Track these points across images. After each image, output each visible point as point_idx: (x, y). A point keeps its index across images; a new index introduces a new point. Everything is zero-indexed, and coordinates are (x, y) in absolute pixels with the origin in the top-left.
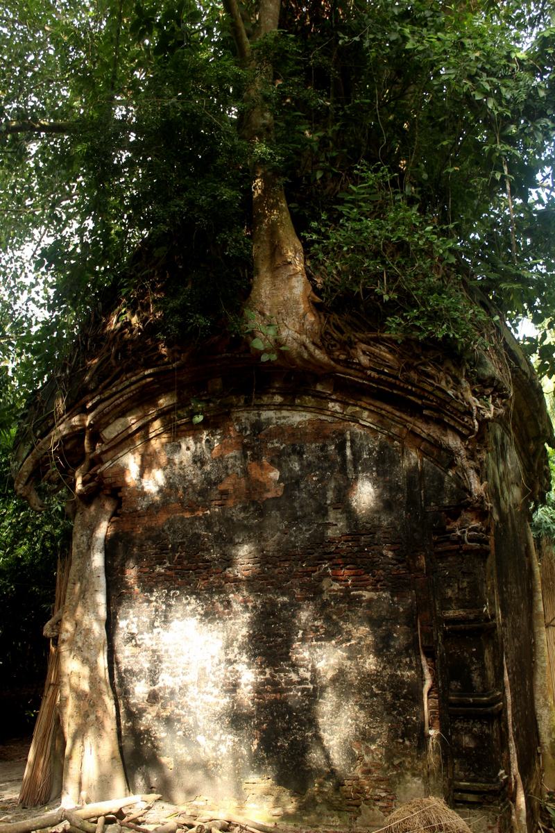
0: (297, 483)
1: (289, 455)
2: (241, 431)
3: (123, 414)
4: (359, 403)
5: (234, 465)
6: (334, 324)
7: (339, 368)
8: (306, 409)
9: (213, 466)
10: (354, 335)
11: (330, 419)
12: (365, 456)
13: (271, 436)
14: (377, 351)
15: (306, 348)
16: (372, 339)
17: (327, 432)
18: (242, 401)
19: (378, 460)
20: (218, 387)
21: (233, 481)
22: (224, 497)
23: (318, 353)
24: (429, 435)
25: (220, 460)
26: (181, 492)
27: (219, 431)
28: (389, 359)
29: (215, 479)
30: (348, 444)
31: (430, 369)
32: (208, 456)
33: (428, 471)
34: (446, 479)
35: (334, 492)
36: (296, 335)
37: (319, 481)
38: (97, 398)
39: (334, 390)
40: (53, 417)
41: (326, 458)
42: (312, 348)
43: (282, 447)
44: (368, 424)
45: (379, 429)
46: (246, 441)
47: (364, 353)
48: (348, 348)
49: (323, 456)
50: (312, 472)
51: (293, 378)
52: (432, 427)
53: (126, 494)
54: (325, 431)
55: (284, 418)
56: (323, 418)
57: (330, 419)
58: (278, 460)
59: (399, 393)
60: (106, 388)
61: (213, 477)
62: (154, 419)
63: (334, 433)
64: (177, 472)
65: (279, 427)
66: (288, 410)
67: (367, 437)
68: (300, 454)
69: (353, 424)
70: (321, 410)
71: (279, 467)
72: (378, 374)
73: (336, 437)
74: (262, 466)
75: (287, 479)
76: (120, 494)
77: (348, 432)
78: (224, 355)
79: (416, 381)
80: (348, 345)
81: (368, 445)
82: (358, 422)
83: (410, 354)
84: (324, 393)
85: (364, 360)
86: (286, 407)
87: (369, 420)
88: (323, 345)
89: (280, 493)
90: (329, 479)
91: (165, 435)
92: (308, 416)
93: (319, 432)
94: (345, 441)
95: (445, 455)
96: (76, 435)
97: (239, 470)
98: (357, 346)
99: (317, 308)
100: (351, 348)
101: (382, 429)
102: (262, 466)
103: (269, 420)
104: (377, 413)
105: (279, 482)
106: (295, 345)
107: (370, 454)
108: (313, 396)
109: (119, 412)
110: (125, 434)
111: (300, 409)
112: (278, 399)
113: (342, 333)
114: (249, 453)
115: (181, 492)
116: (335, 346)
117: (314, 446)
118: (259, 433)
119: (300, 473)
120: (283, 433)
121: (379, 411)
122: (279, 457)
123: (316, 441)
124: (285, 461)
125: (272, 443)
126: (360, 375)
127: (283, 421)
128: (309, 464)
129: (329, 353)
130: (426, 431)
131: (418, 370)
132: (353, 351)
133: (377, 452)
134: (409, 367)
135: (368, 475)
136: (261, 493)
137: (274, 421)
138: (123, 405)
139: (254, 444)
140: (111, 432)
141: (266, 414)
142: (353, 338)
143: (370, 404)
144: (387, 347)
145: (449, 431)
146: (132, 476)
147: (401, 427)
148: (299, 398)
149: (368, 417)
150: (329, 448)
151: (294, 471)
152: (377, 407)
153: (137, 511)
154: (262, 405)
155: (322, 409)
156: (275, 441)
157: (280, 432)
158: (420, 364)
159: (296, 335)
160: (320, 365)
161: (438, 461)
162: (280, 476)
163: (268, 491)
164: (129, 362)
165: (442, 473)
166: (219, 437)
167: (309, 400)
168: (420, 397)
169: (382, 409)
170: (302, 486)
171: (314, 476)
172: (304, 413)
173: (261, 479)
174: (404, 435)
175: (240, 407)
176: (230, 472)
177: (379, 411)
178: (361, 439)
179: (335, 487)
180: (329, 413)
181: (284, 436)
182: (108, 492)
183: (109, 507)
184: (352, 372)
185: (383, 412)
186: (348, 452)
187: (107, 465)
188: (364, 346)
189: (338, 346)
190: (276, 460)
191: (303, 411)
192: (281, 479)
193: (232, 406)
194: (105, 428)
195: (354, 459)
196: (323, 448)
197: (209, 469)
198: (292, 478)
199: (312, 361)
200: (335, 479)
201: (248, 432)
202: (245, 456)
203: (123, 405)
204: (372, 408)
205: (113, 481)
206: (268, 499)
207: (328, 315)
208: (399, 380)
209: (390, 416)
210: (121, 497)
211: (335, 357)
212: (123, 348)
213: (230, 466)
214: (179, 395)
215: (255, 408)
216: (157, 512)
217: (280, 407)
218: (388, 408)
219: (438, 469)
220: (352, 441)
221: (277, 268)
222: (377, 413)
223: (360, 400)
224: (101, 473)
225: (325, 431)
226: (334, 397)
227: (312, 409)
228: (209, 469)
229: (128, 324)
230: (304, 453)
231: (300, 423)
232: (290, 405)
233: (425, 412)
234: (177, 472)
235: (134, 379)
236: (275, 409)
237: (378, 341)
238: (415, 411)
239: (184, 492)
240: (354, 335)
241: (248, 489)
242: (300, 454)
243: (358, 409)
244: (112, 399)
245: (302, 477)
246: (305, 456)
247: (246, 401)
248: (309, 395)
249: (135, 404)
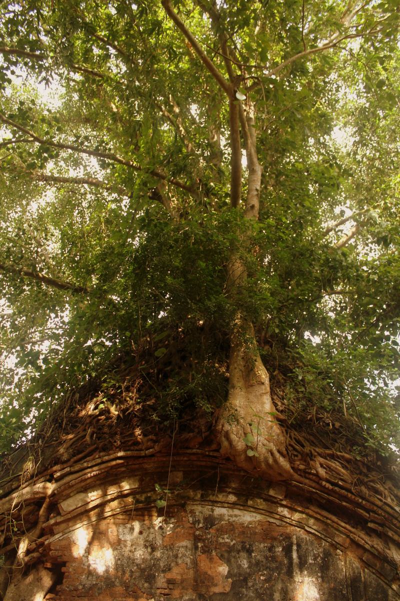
0: (245, 580)
1: (238, 552)
2: (194, 523)
3: (86, 489)
4: (307, 511)
5: (184, 555)
6: (295, 439)
7: (296, 476)
8: (257, 510)
9: (163, 553)
10: (314, 450)
11: (278, 522)
12: (310, 561)
13: (221, 531)
14: (334, 465)
15: (272, 454)
16: (329, 455)
17: (275, 534)
18: (199, 496)
19: (322, 566)
20: (178, 480)
21: (182, 571)
22: (171, 586)
23: (281, 460)
24: (372, 547)
25: (171, 548)
26: (127, 575)
27: (173, 520)
28: (344, 474)
29: (164, 566)
30: (295, 547)
31: (379, 486)
32: (159, 542)
33: (371, 582)
34: (390, 592)
35: (281, 593)
36: (265, 442)
37: (266, 581)
38: (68, 469)
39: (285, 497)
40: (19, 480)
41: (274, 558)
42: (277, 455)
43: (232, 544)
44: (313, 531)
45: (323, 536)
46: (197, 533)
47: (322, 466)
48: (309, 459)
49: (271, 557)
50: (259, 570)
51: (253, 482)
52: (375, 539)
53: (71, 570)
54: (273, 533)
55: (236, 516)
56: (272, 520)
57: (278, 522)
58: (228, 554)
59: (347, 505)
60: (76, 462)
61: (162, 565)
62: (113, 500)
63: (281, 536)
64: (126, 555)
65: (231, 524)
66: (240, 509)
67: (312, 543)
68: (249, 552)
69: (299, 529)
70: (271, 513)
71: (228, 562)
72: (332, 485)
73: (284, 540)
74: (211, 560)
75: (235, 576)
76: (64, 569)
77: (295, 537)
78: (194, 451)
79: (367, 495)
80: (308, 458)
81: (313, 550)
82: (303, 528)
83: (358, 472)
84: (276, 498)
85: (322, 472)
86: (239, 507)
87: (314, 527)
88: (288, 453)
89: (228, 589)
90: (276, 579)
91: (121, 517)
92: (259, 517)
93: (268, 534)
94: (291, 545)
95: (389, 568)
96: (37, 502)
97: (188, 561)
98: (315, 459)
99: (281, 423)
100: (311, 460)
101: (326, 537)
102: (211, 560)
103: (221, 517)
104: (323, 522)
105: (227, 577)
106: (264, 450)
107: (315, 559)
108: (265, 500)
109: (82, 487)
110: (82, 509)
111: (252, 509)
112: (232, 498)
113: (303, 446)
114: (200, 545)
115: (127, 575)
116: (297, 456)
117: (262, 545)
118: (211, 527)
119: (248, 570)
120: (233, 530)
121: (325, 520)
122: (229, 552)
123: (264, 541)
124: (234, 557)
125: (223, 538)
126: (314, 484)
127: (234, 519)
128: (258, 563)
129: (291, 462)
130: (369, 543)
131: (367, 486)
132: (311, 462)
133: (322, 558)
134: (360, 482)
135: (314, 580)
136: (208, 587)
137: (226, 518)
138: (89, 481)
139: (204, 540)
140: (68, 505)
141: (219, 511)
142: (313, 451)
143: (317, 513)
144: (341, 464)
145: (391, 545)
146: (78, 551)
147: (344, 537)
148: (251, 499)
149: (314, 525)
150: (277, 550)
151: (243, 568)
152: (325, 517)
153: (78, 590)
154: (217, 502)
155: (272, 513)
156: (226, 536)
157: (231, 528)
158: (370, 481)
159: (265, 442)
160: (281, 471)
161: (380, 574)
162: (229, 572)
163: (216, 585)
164: (106, 443)
165: (385, 586)
166: (172, 526)
167: (260, 503)
168: (368, 511)
169: (327, 518)
170: (250, 584)
171: (261, 575)
172: (254, 514)
173: (209, 572)
174: (347, 545)
175: (196, 500)
176: (180, 561)
177: (325, 520)
178: (306, 544)
179: (282, 588)
180: (278, 517)
181: (234, 533)
182: (49, 565)
183: (47, 581)
184: (307, 481)
185: (329, 521)
186: (295, 555)
187: (57, 536)
188: (322, 460)
189: (300, 456)
190: (226, 555)
191: (254, 512)
192: (230, 575)
193: (189, 498)
194: (64, 500)
195: (300, 563)
196: (271, 549)
197: (159, 555)
198: (240, 575)
199: (275, 466)
200: (282, 580)
201: (201, 525)
202: (196, 548)
203: (89, 481)
204: (319, 517)
205: (60, 554)
206: (215, 594)
207: (289, 431)
208: (352, 493)
209: (335, 525)
210: (64, 573)
211: (296, 466)
212: (99, 429)
213: (180, 555)
214: (141, 481)
215: (210, 503)
216: (99, 594)
217: (233, 506)
218: (335, 518)
219: (380, 581)
220: (299, 545)
221: (252, 386)
222: (323, 522)
223: (308, 508)
224: (49, 544)
225: (273, 533)
226: (284, 503)
227: (263, 512)
228: (159, 555)
229: (107, 411)
230: (253, 551)
231: (250, 523)
232: (242, 504)
233: (370, 525)
234: (126, 555)
235: (106, 458)
236: (228, 507)
237: (333, 457)
238: (360, 522)
239: (131, 576)
240: (314, 450)
241: (196, 581)
242: (249, 552)
243: (304, 516)
244: (81, 474)
245: (250, 575)
246: (253, 555)
247: (202, 496)
248: (262, 498)
249: (98, 482)
